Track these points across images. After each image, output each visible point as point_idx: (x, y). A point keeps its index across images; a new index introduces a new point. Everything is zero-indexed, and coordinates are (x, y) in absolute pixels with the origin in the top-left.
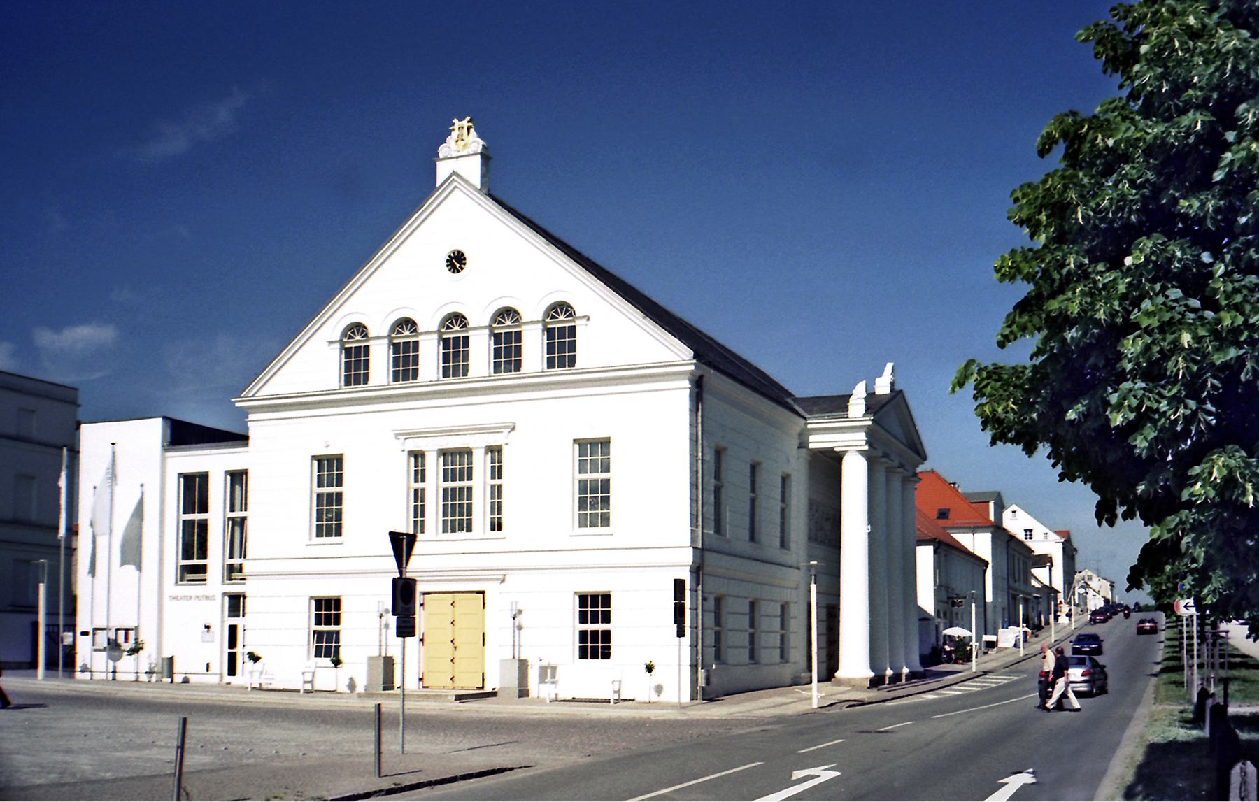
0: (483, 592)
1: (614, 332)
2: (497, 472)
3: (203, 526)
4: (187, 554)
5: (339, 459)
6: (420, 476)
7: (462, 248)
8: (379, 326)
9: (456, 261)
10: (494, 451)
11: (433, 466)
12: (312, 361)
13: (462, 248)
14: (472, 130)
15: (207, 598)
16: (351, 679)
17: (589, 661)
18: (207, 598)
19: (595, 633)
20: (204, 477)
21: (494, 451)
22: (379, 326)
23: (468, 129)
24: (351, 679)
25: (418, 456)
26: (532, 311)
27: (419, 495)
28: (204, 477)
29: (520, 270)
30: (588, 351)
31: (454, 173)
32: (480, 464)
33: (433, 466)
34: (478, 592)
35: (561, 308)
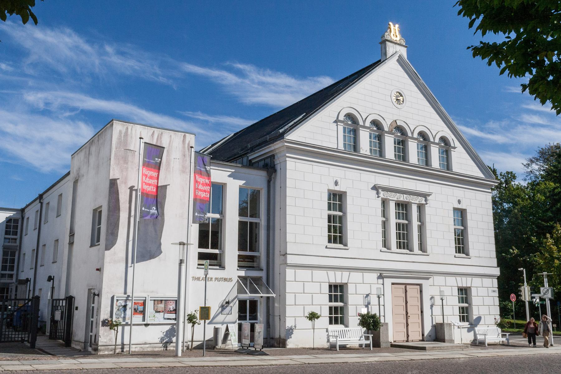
0: (420, 285)
10: (421, 208)
15: (225, 280)
18: (225, 280)
21: (421, 208)
25: (384, 203)
27: (385, 225)
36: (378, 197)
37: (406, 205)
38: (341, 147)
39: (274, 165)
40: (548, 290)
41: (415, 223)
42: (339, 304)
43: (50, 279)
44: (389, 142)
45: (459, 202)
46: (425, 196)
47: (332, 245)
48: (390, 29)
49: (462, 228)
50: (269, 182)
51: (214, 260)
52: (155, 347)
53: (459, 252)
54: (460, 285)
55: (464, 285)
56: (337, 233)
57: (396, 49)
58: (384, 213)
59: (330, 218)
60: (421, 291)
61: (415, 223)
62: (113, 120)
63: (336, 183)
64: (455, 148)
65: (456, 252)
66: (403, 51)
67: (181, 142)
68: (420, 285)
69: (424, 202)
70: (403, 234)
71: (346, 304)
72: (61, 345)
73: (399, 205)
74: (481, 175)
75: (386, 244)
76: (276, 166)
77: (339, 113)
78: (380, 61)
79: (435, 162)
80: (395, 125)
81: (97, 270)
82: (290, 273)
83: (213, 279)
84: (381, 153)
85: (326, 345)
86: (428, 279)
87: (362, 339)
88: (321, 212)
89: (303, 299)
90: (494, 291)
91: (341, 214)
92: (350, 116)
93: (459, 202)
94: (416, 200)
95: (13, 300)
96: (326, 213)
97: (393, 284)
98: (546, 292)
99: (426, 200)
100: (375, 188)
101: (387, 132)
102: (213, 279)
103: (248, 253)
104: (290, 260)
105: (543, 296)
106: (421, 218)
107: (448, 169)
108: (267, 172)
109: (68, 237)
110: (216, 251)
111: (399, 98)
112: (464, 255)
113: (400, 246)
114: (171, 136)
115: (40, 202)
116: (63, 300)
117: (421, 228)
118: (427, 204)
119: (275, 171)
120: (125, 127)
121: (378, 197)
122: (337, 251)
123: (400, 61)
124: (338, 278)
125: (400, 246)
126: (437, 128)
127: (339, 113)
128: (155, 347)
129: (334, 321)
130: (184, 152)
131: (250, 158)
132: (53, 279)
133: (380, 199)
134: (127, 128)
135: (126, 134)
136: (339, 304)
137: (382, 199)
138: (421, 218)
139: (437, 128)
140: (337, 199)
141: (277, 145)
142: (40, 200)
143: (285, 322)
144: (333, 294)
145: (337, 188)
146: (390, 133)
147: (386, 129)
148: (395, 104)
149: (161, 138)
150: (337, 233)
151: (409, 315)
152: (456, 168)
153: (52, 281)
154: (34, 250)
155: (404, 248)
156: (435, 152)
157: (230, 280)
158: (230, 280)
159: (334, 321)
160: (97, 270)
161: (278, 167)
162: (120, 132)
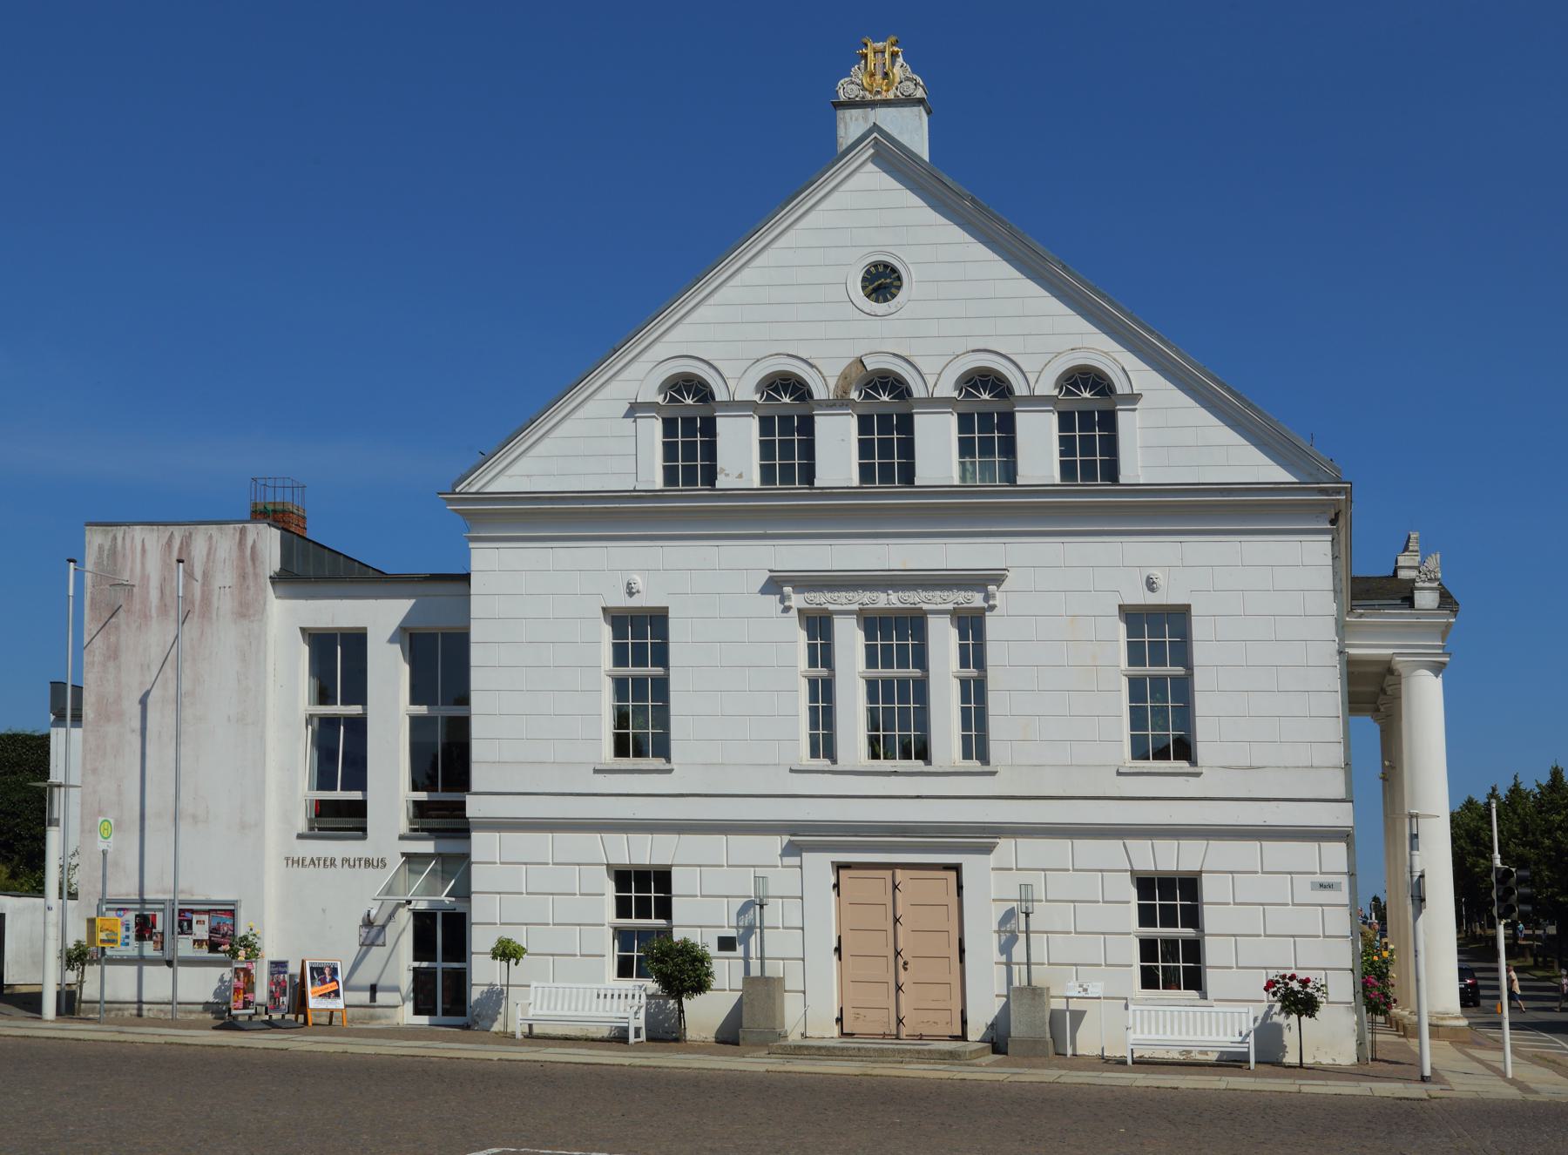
0: (957, 868)
1: (1171, 435)
2: (974, 654)
3: (358, 727)
4: (325, 780)
5: (657, 620)
6: (822, 654)
7: (862, 270)
8: (738, 382)
9: (882, 282)
10: (971, 625)
11: (850, 641)
12: (599, 438)
13: (862, 270)
14: (900, 60)
15: (368, 863)
16: (1376, 899)
17: (1161, 993)
18: (368, 863)
19: (1170, 944)
20: (355, 641)
21: (971, 625)
22: (738, 382)
23: (894, 55)
24: (1376, 899)
25: (819, 625)
26: (1037, 374)
27: (823, 692)
28: (355, 641)
29: (982, 310)
30: (1135, 466)
31: (876, 127)
32: (944, 642)
33: (850, 641)
34: (947, 867)
35: (1084, 378)
36: (787, 609)
46: (983, 581)
47: (629, 762)
51: (340, 817)
52: (191, 1012)
60: (960, 888)
63: (1151, 585)
64: (1134, 398)
67: (235, 548)
68: (957, 868)
73: (872, 623)
75: (824, 745)
80: (856, 373)
83: (338, 862)
86: (988, 850)
89: (1253, 951)
97: (839, 867)
100: (774, 585)
101: (829, 404)
103: (339, 795)
106: (974, 654)
110: (356, 795)
114: (211, 537)
117: (975, 693)
118: (992, 608)
120: (110, 536)
121: (787, 609)
124: (643, 852)
128: (191, 1012)
130: (243, 569)
133: (794, 613)
134: (115, 538)
135: (113, 551)
140: (641, 634)
146: (839, 403)
147: (819, 393)
149: (188, 545)
157: (382, 863)
158: (382, 863)
162: (101, 547)
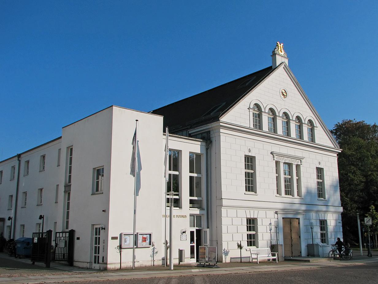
15: (182, 216)
18: (182, 216)
21: (298, 166)
25: (277, 163)
27: (278, 178)
37: (251, 159)
38: (252, 126)
39: (210, 138)
40: (370, 220)
41: (295, 178)
42: (253, 232)
43: (41, 217)
44: (306, 129)
45: (320, 163)
46: (301, 159)
48: (278, 46)
49: (290, 177)
50: (207, 149)
53: (249, 191)
54: (249, 217)
55: (252, 217)
56: (250, 184)
57: (281, 58)
58: (278, 171)
59: (318, 183)
61: (295, 178)
62: (112, 106)
63: (250, 151)
64: (316, 127)
65: (246, 191)
66: (286, 61)
69: (299, 163)
70: (288, 184)
71: (257, 232)
72: (65, 265)
74: (333, 146)
75: (279, 192)
76: (211, 139)
77: (251, 102)
78: (271, 67)
79: (306, 137)
81: (103, 211)
82: (224, 211)
83: (175, 216)
84: (275, 131)
85: (98, 269)
87: (270, 255)
88: (241, 170)
90: (339, 222)
91: (252, 171)
92: (257, 105)
93: (320, 163)
94: (295, 163)
95: (41, 233)
96: (244, 171)
98: (368, 221)
99: (301, 162)
102: (175, 216)
104: (225, 202)
105: (366, 223)
107: (288, 135)
108: (206, 143)
109: (64, 188)
111: (284, 94)
112: (253, 193)
113: (287, 193)
115: (18, 160)
116: (60, 233)
119: (211, 142)
122: (250, 196)
123: (285, 68)
125: (287, 193)
126: (307, 114)
127: (251, 102)
129: (250, 244)
131: (190, 133)
132: (43, 218)
133: (275, 161)
136: (253, 232)
137: (276, 161)
138: (298, 174)
139: (307, 114)
140: (250, 161)
141: (214, 125)
142: (18, 158)
143: (222, 245)
144: (249, 225)
145: (250, 154)
148: (283, 99)
150: (250, 184)
151: (292, 239)
152: (317, 141)
153: (11, 220)
154: (12, 196)
155: (288, 195)
156: (306, 129)
159: (250, 244)
160: (103, 211)
161: (213, 140)
